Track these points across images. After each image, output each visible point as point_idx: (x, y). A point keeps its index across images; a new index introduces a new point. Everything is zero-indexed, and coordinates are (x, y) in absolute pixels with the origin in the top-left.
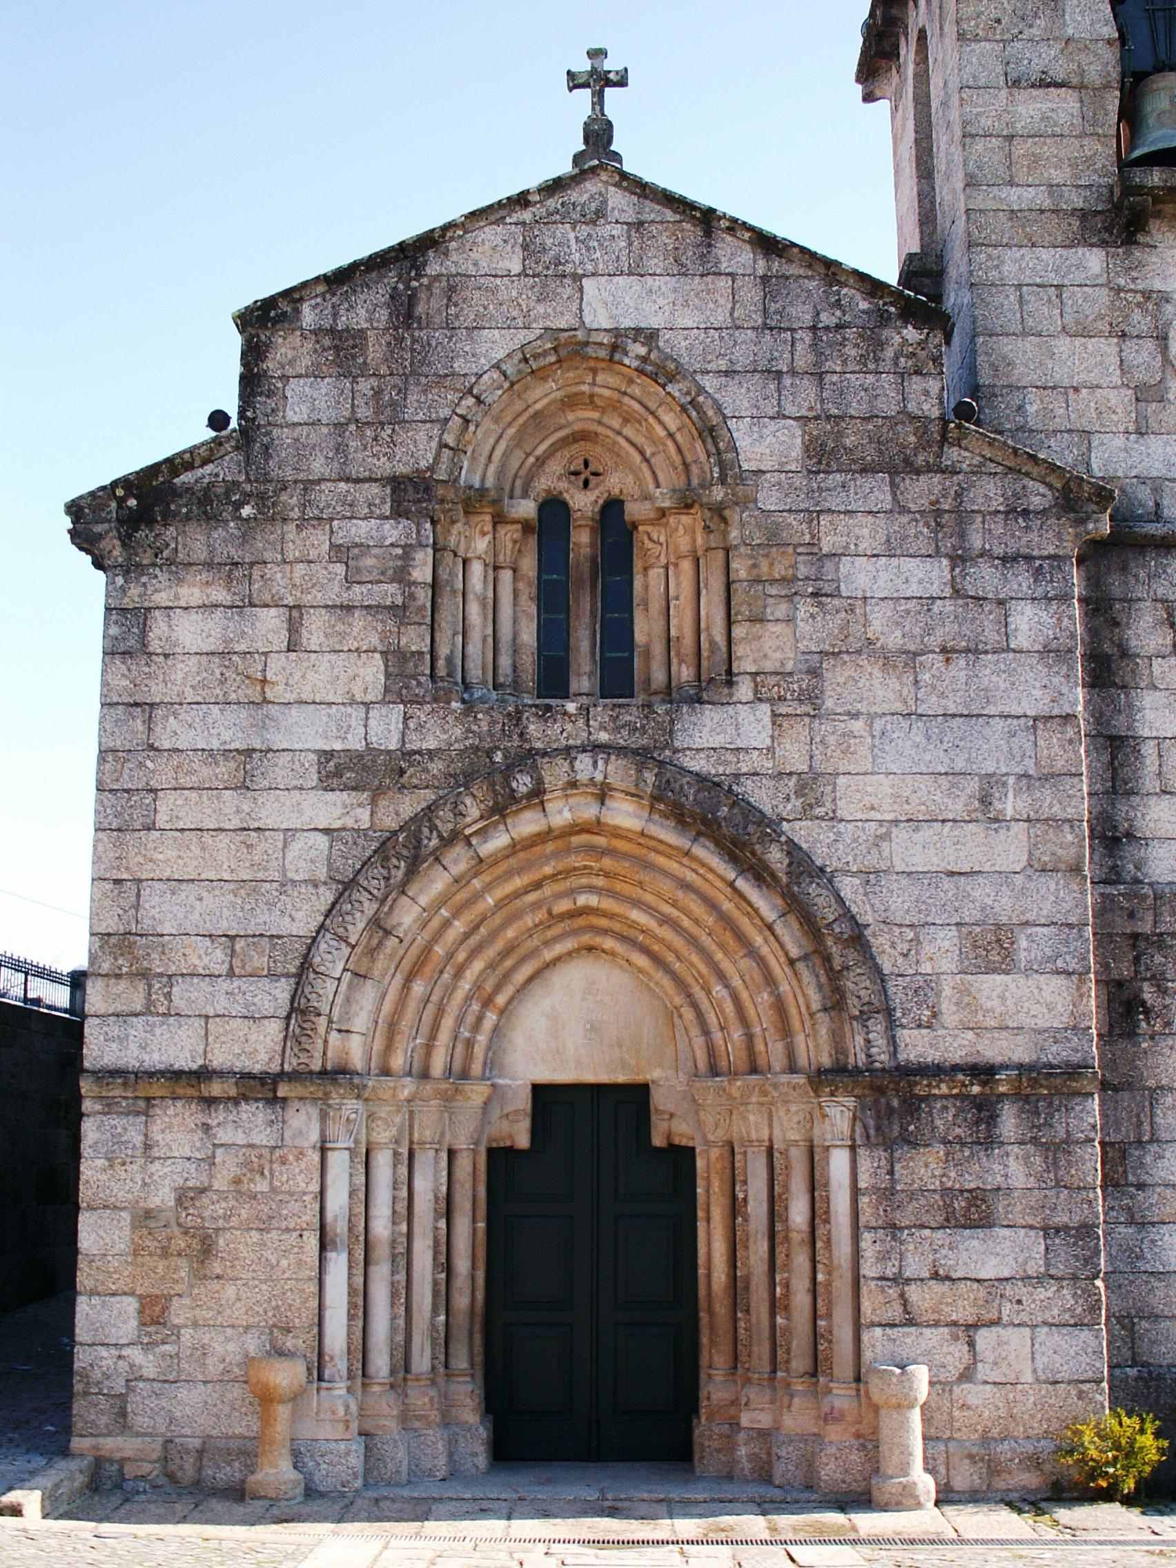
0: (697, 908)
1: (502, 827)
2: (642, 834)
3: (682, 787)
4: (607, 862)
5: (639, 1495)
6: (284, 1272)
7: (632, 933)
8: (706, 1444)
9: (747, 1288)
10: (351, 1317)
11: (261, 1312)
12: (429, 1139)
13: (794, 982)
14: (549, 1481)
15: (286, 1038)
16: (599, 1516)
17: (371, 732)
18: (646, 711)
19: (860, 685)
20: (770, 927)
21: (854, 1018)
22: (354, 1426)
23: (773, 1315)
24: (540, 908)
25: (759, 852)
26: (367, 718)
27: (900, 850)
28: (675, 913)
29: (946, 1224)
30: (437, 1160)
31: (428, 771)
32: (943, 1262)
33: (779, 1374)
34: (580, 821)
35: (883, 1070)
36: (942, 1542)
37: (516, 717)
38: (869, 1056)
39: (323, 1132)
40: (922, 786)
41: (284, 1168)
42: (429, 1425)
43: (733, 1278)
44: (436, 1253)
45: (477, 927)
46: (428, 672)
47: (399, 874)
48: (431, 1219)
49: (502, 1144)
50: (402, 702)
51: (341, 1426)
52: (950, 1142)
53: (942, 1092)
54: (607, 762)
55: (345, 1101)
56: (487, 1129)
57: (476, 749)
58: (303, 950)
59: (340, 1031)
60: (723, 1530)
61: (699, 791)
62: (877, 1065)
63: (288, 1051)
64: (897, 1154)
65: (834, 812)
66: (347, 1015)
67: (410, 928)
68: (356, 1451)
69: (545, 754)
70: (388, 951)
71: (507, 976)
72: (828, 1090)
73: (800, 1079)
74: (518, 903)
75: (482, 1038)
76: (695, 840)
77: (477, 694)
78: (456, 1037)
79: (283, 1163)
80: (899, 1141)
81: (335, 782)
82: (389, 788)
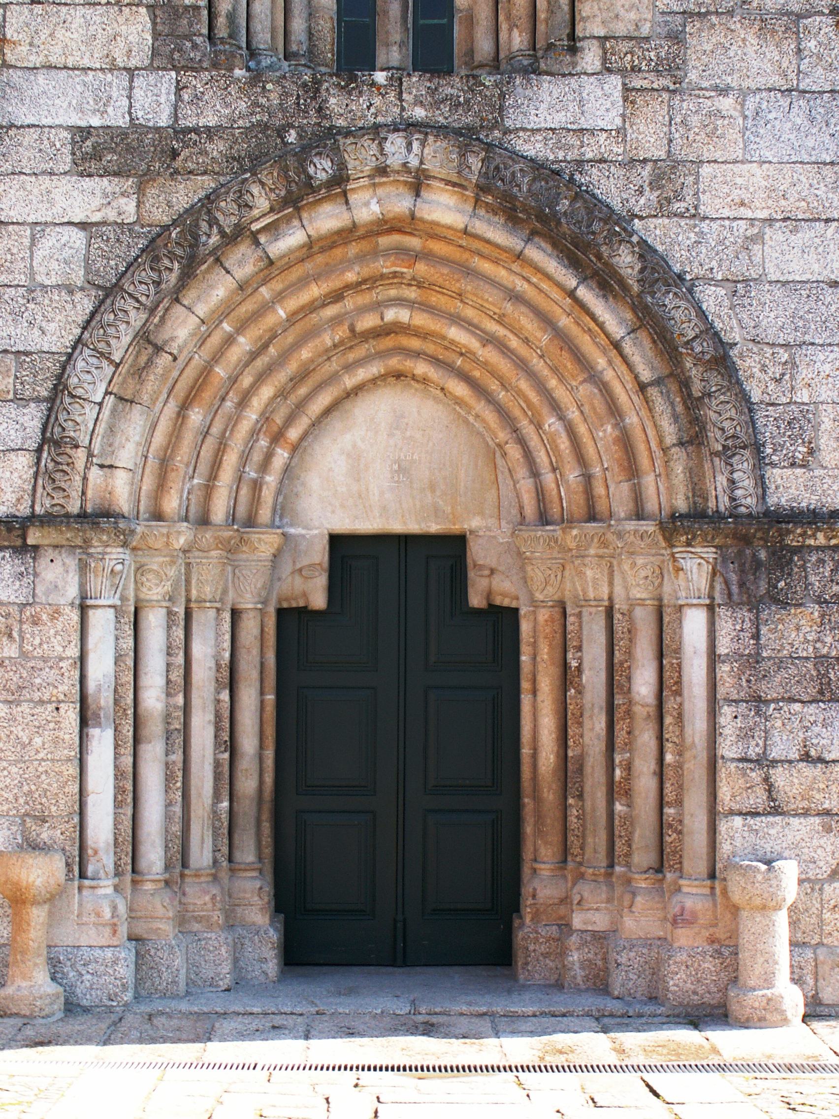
0: (528, 324)
1: (296, 222)
2: (465, 231)
3: (513, 174)
4: (421, 268)
5: (456, 1008)
6: (37, 752)
7: (450, 356)
8: (531, 947)
9: (580, 770)
10: (118, 804)
11: (11, 798)
12: (209, 597)
13: (644, 413)
14: (351, 992)
15: (36, 475)
16: (412, 1034)
17: (137, 105)
18: (472, 82)
19: (731, 53)
20: (617, 346)
21: (717, 454)
22: (123, 930)
23: (610, 802)
24: (341, 323)
25: (605, 255)
26: (131, 88)
27: (775, 255)
28: (501, 331)
29: (819, 697)
30: (218, 620)
31: (207, 153)
32: (815, 741)
33: (618, 869)
34: (391, 215)
35: (750, 515)
36: (824, 1068)
37: (314, 89)
38: (733, 499)
39: (82, 586)
40: (802, 178)
41: (36, 629)
42: (210, 927)
43: (563, 757)
44: (218, 729)
45: (266, 346)
46: (205, 31)
47: (172, 278)
48: (212, 689)
49: (294, 605)
50: (174, 68)
51: (108, 931)
52: (826, 602)
53: (818, 543)
54: (423, 144)
55: (109, 550)
56: (277, 585)
57: (264, 127)
58: (56, 369)
59: (102, 466)
60: (561, 1052)
61: (534, 180)
62: (743, 510)
63: (40, 490)
64: (764, 615)
65: (696, 207)
66: (109, 446)
67: (186, 343)
68: (126, 959)
69: (348, 133)
70: (159, 370)
71: (301, 406)
72: (684, 538)
73: (649, 527)
74: (314, 318)
75: (271, 479)
76: (528, 240)
77: (265, 62)
78: (240, 479)
79: (35, 623)
80: (766, 600)
81: (93, 166)
82: (158, 174)
